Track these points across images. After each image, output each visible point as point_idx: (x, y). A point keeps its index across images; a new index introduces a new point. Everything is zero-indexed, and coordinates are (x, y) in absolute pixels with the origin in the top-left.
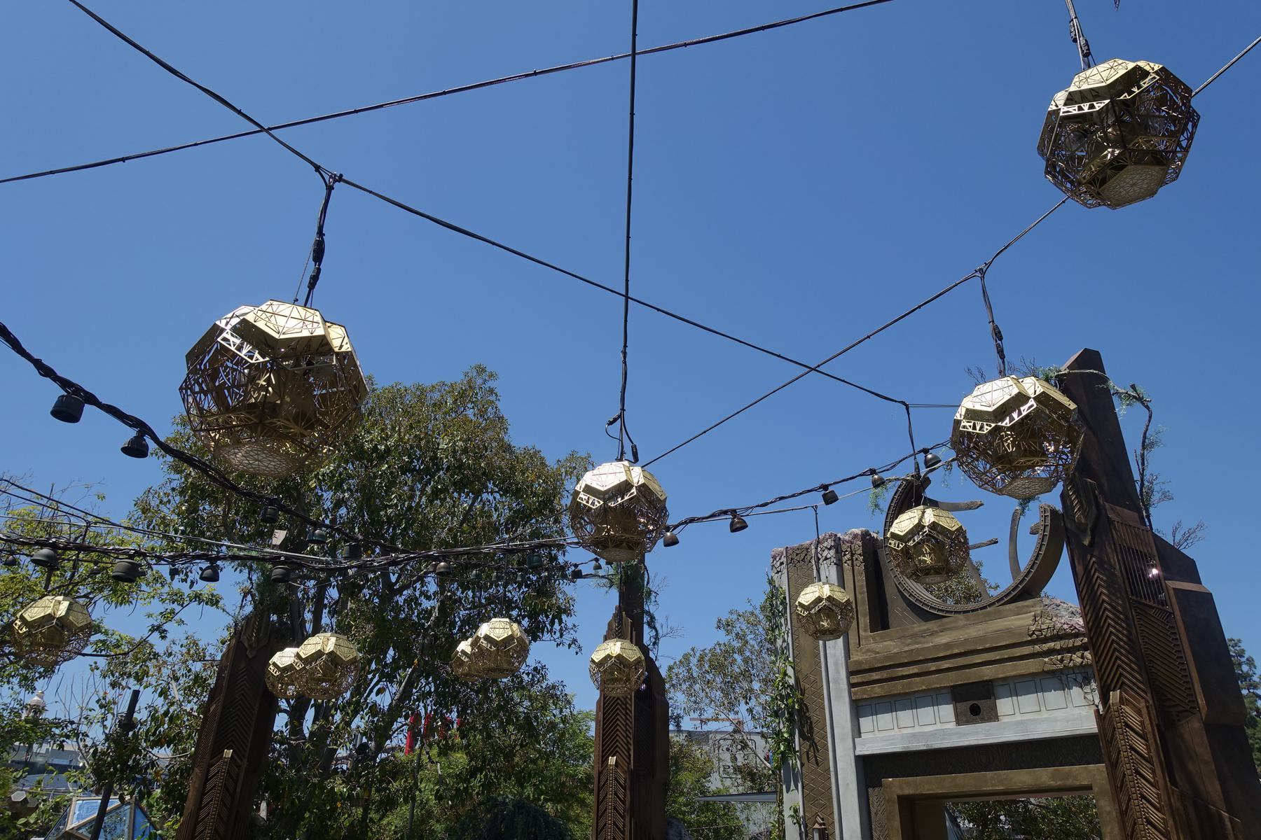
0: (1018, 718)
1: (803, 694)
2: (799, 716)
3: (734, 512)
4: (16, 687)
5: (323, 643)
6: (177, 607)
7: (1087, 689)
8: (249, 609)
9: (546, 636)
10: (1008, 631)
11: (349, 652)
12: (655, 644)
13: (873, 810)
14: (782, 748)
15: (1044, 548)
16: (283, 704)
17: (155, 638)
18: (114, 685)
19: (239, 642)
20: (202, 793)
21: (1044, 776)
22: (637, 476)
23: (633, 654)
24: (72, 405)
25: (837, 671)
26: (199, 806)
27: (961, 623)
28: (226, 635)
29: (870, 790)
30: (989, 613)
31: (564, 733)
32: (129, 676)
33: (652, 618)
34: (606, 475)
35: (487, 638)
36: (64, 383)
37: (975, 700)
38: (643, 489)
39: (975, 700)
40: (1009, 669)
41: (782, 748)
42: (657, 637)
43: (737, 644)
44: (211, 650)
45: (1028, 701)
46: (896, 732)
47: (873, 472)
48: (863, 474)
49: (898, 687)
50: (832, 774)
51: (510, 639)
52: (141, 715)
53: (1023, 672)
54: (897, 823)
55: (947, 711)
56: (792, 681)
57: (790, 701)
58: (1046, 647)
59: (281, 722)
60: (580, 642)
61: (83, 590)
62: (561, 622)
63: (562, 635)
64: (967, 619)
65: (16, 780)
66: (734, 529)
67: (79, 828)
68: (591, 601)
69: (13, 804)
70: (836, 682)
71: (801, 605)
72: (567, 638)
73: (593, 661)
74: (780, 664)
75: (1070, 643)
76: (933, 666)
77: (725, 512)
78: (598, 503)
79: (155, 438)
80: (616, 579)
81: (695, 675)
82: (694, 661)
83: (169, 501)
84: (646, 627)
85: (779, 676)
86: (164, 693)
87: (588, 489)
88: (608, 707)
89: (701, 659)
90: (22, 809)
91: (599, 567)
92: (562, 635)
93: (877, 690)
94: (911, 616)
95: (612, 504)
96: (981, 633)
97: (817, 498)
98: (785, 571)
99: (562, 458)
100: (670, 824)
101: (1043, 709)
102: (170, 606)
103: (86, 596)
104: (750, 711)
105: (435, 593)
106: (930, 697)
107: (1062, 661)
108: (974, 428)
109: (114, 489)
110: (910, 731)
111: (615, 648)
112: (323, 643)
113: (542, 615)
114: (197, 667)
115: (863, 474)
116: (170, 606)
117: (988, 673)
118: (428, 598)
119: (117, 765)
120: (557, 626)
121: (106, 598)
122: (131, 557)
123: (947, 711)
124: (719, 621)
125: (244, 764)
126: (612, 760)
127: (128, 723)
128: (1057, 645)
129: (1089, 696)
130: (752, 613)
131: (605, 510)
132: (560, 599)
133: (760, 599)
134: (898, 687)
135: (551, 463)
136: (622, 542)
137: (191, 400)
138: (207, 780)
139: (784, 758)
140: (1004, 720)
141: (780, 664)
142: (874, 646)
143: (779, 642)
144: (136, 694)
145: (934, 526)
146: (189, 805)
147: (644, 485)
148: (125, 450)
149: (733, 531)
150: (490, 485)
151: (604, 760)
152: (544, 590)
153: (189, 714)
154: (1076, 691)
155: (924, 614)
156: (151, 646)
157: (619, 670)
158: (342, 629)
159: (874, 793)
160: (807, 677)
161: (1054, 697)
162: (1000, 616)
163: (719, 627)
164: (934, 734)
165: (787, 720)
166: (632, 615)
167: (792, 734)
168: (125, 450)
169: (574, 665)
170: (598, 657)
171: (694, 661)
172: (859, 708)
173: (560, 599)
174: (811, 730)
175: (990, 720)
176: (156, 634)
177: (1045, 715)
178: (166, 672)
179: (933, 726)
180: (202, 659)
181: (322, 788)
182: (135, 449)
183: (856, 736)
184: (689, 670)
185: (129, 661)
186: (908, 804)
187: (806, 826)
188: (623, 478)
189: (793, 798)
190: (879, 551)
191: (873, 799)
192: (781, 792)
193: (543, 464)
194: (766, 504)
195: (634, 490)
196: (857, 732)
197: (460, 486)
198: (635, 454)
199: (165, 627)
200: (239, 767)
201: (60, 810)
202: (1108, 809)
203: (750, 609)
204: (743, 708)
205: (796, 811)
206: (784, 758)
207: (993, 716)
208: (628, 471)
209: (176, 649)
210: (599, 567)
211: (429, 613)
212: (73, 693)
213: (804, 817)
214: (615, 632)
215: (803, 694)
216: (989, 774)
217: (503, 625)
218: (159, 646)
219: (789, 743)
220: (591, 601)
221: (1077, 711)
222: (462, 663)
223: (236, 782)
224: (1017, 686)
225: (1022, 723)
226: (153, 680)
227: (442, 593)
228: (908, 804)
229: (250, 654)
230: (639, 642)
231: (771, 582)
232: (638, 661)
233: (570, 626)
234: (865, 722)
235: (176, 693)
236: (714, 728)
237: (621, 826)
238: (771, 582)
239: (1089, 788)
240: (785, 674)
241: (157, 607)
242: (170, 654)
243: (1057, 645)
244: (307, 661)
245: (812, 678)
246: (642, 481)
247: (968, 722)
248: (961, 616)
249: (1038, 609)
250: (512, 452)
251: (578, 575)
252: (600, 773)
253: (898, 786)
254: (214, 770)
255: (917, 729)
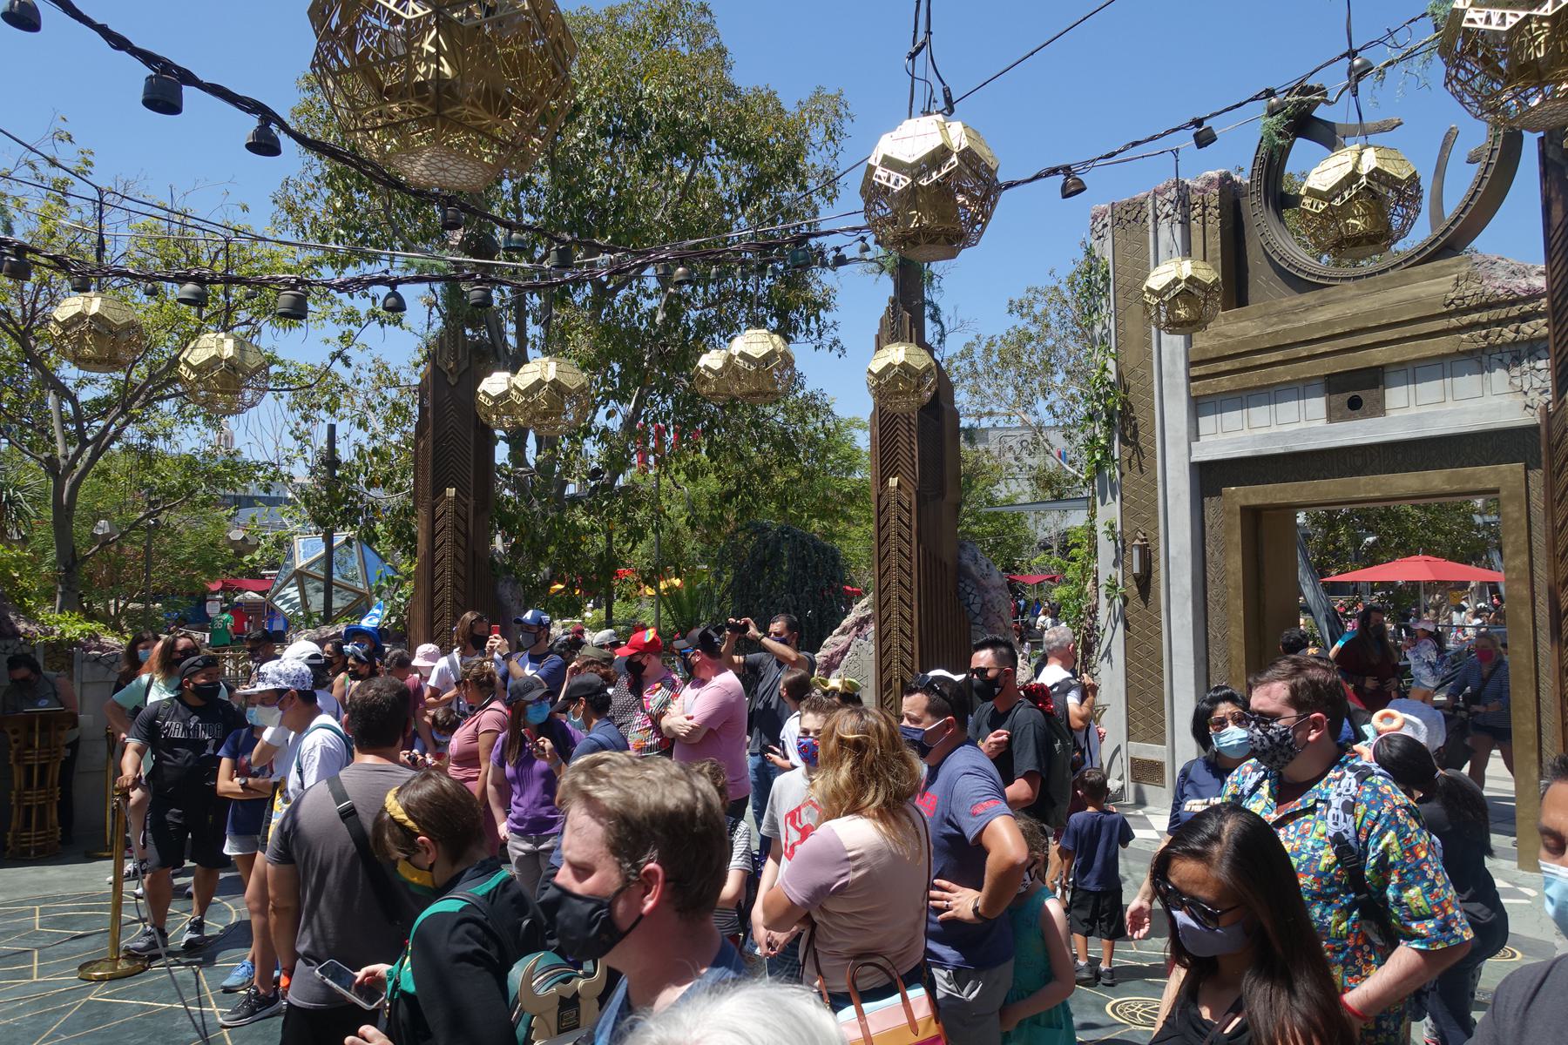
0: (1413, 411)
1: (1126, 392)
2: (1122, 419)
3: (1067, 170)
4: (202, 428)
5: (540, 368)
6: (356, 330)
7: (1516, 372)
8: (438, 324)
9: (801, 337)
10: (1417, 301)
11: (575, 378)
12: (940, 342)
13: (1208, 523)
14: (1098, 457)
15: (1485, 182)
16: (499, 433)
17: (338, 366)
18: (306, 418)
19: (435, 368)
20: (433, 536)
21: (1436, 479)
22: (957, 136)
23: (920, 360)
24: (166, 89)
25: (1173, 362)
26: (433, 549)
27: (1351, 293)
28: (418, 358)
29: (1206, 500)
30: (1391, 279)
31: (829, 444)
32: (320, 407)
33: (936, 309)
34: (914, 138)
35: (743, 355)
36: (147, 58)
37: (1355, 390)
38: (968, 156)
39: (1355, 390)
40: (1410, 351)
41: (1098, 457)
42: (943, 335)
43: (1033, 330)
44: (404, 374)
45: (1430, 390)
46: (1247, 433)
47: (1270, 93)
48: (1256, 98)
49: (1254, 379)
50: (1160, 484)
51: (772, 354)
52: (345, 453)
53: (1428, 353)
54: (1237, 537)
55: (1317, 405)
56: (1113, 377)
57: (1110, 401)
58: (1466, 320)
59: (502, 453)
60: (843, 342)
61: (243, 315)
62: (818, 319)
63: (820, 336)
64: (1359, 287)
65: (229, 518)
66: (1067, 193)
67: (309, 565)
68: (858, 294)
69: (233, 543)
70: (1171, 375)
71: (1150, 290)
72: (827, 338)
73: (870, 372)
74: (1098, 357)
75: (1502, 313)
76: (1303, 351)
77: (1055, 171)
78: (905, 182)
79: (284, 126)
80: (889, 263)
81: (980, 368)
82: (978, 351)
83: (315, 194)
84: (928, 321)
85: (1097, 372)
86: (362, 424)
87: (888, 162)
88: (885, 424)
89: (988, 350)
90: (243, 547)
91: (867, 249)
92: (820, 336)
93: (1226, 383)
94: (1278, 285)
95: (924, 182)
96: (1377, 306)
97: (1186, 139)
98: (1109, 236)
99: (805, 98)
100: (962, 547)
101: (1449, 398)
102: (346, 328)
103: (248, 323)
104: (1050, 408)
105: (657, 291)
106: (1298, 389)
107: (1486, 337)
108: (1488, 20)
109: (245, 196)
110: (1265, 431)
111: (897, 354)
112: (540, 368)
113: (791, 310)
114: (392, 394)
115: (1256, 98)
116: (346, 328)
117: (1379, 356)
118: (649, 297)
119: (333, 500)
120: (813, 325)
121: (272, 323)
122: (294, 287)
123: (1317, 405)
124: (1011, 303)
125: (471, 502)
126: (893, 482)
127: (330, 460)
128: (1483, 317)
129: (1517, 382)
130: (1056, 289)
131: (912, 192)
132: (816, 291)
133: (1066, 269)
134: (1254, 379)
135: (790, 107)
136: (939, 234)
137: (330, 83)
138: (434, 522)
139: (1099, 467)
140: (1392, 414)
141: (1098, 357)
142: (1225, 328)
143: (1098, 328)
144: (332, 428)
145: (1377, 174)
146: (422, 546)
147: (968, 149)
148: (250, 147)
149: (1065, 196)
150: (713, 146)
151: (884, 482)
152: (795, 280)
153: (396, 447)
154: (1499, 375)
155: (1298, 282)
156: (337, 377)
157: (905, 381)
158: (554, 344)
159: (1211, 504)
160: (1133, 370)
161: (1467, 383)
162: (1406, 281)
163: (1011, 311)
164: (1296, 435)
165: (1105, 424)
166: (909, 313)
167: (1110, 440)
168: (250, 147)
169: (844, 373)
170: (877, 366)
171: (978, 351)
172: (1199, 406)
173: (816, 291)
174: (1135, 434)
175: (1373, 415)
176: (338, 361)
177: (1450, 406)
178: (359, 401)
179: (1302, 424)
180: (396, 385)
181: (562, 522)
182: (264, 145)
183: (1184, 440)
184: (972, 364)
185: (316, 392)
186: (1253, 517)
187: (1124, 542)
188: (937, 141)
189: (1110, 512)
190: (1243, 201)
191: (1209, 512)
192: (1094, 506)
193: (780, 111)
194: (1113, 155)
195: (954, 159)
196: (1195, 434)
197: (674, 152)
198: (949, 101)
199: (347, 353)
200: (466, 506)
201: (282, 543)
202: (1516, 515)
203: (1054, 283)
204: (1041, 406)
205: (1112, 526)
206: (1099, 467)
207: (1379, 409)
208: (944, 129)
209: (364, 374)
210: (867, 249)
211: (652, 313)
212: (263, 432)
213: (1122, 532)
214: (891, 333)
215: (1126, 392)
216: (1363, 479)
217: (760, 338)
218: (346, 375)
219: (1106, 451)
220: (858, 294)
221: (1496, 400)
222: (706, 381)
223: (466, 522)
224: (1413, 371)
225: (1417, 417)
226: (347, 411)
227: (665, 290)
228: (1253, 517)
229: (452, 381)
230: (922, 344)
231: (1089, 252)
232: (928, 369)
233: (829, 323)
234: (1206, 423)
235: (378, 426)
236: (1016, 433)
237: (907, 552)
238: (1089, 252)
239: (1497, 491)
240: (1105, 369)
241: (333, 331)
242: (359, 382)
243: (1483, 317)
244: (528, 392)
245: (1140, 371)
246: (965, 144)
247: (1343, 419)
248: (1350, 284)
249: (1464, 270)
250: (736, 96)
251: (841, 261)
252: (879, 496)
253: (1242, 495)
254: (439, 511)
255: (1274, 429)
